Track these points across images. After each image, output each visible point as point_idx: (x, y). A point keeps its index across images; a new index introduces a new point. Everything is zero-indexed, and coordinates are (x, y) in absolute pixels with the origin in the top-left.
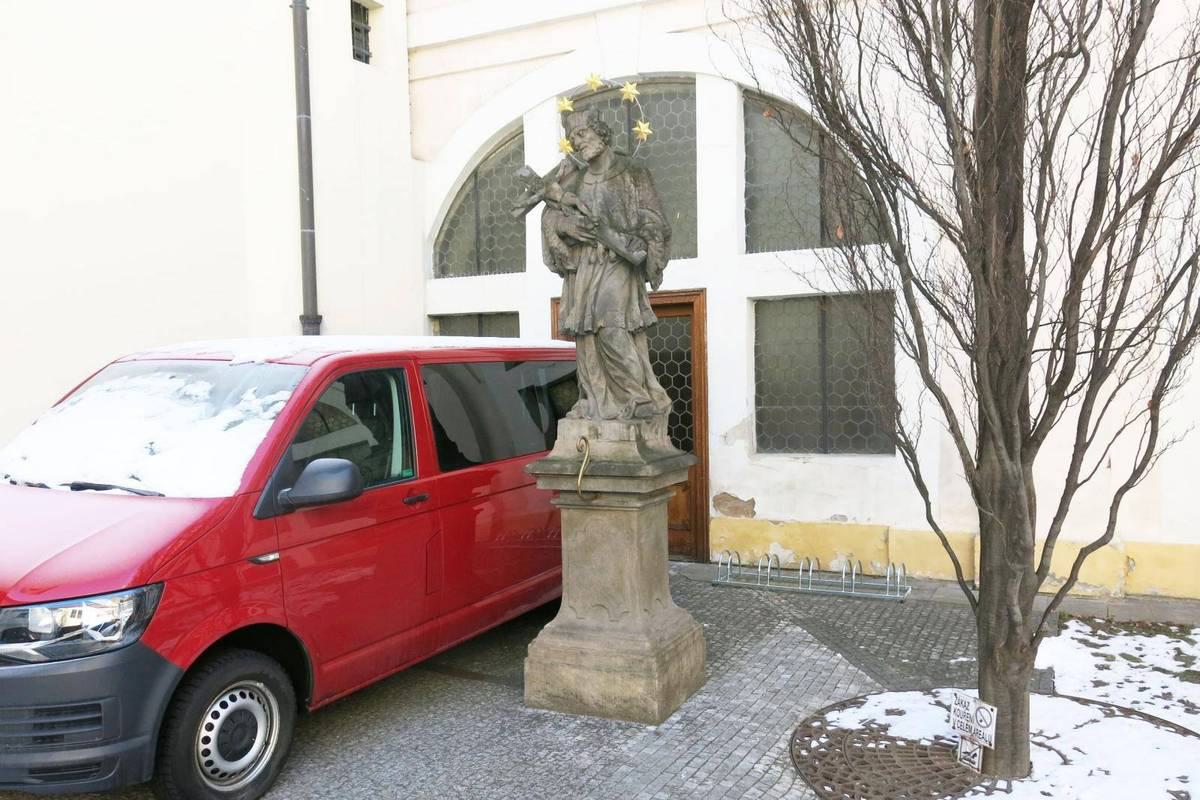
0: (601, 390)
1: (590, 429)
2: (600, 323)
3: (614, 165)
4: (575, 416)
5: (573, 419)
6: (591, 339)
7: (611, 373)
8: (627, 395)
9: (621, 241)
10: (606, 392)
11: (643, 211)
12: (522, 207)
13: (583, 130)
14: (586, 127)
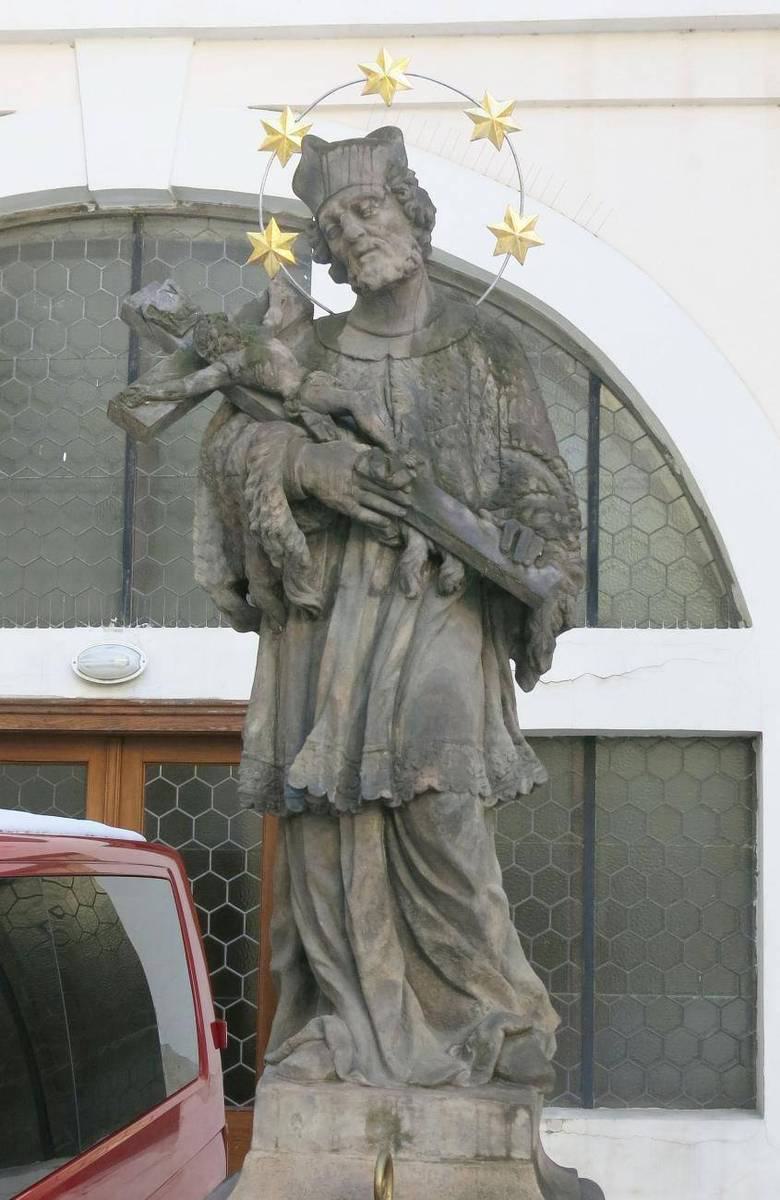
0: (388, 986)
1: (371, 1119)
2: (428, 779)
3: (436, 317)
4: (316, 1072)
5: (310, 1082)
6: (372, 827)
7: (423, 933)
8: (465, 1005)
9: (485, 531)
10: (405, 994)
11: (517, 455)
12: (168, 399)
13: (373, 198)
14: (382, 193)
